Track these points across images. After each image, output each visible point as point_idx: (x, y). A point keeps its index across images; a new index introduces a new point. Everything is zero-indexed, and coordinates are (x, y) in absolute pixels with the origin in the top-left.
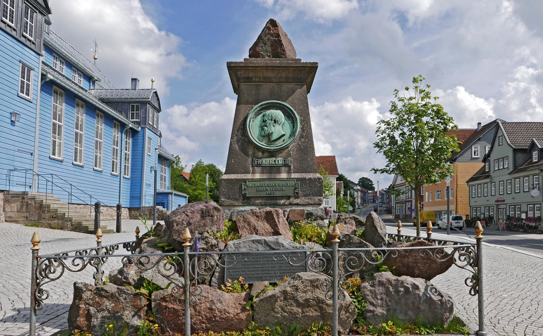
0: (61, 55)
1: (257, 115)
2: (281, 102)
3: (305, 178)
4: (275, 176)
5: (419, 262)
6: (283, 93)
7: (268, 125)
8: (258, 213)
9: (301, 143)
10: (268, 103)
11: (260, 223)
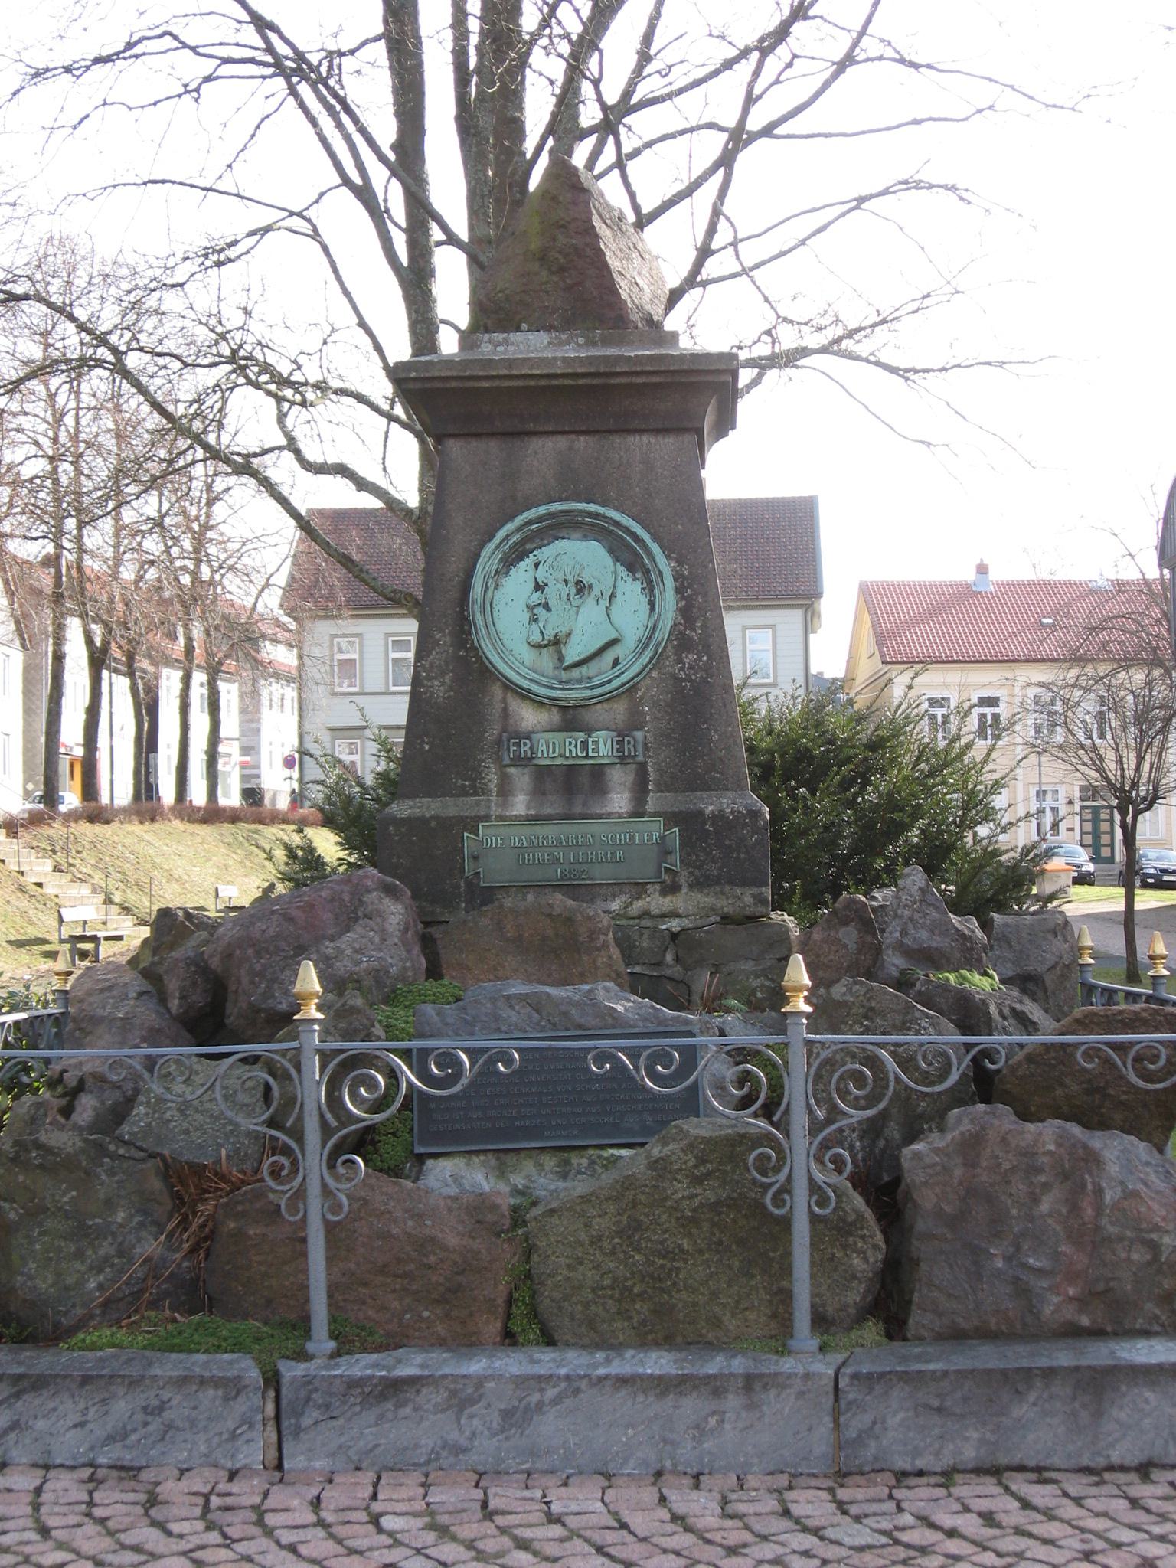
1: (513, 557)
2: (601, 510)
5: (1107, 1082)
10: (551, 515)
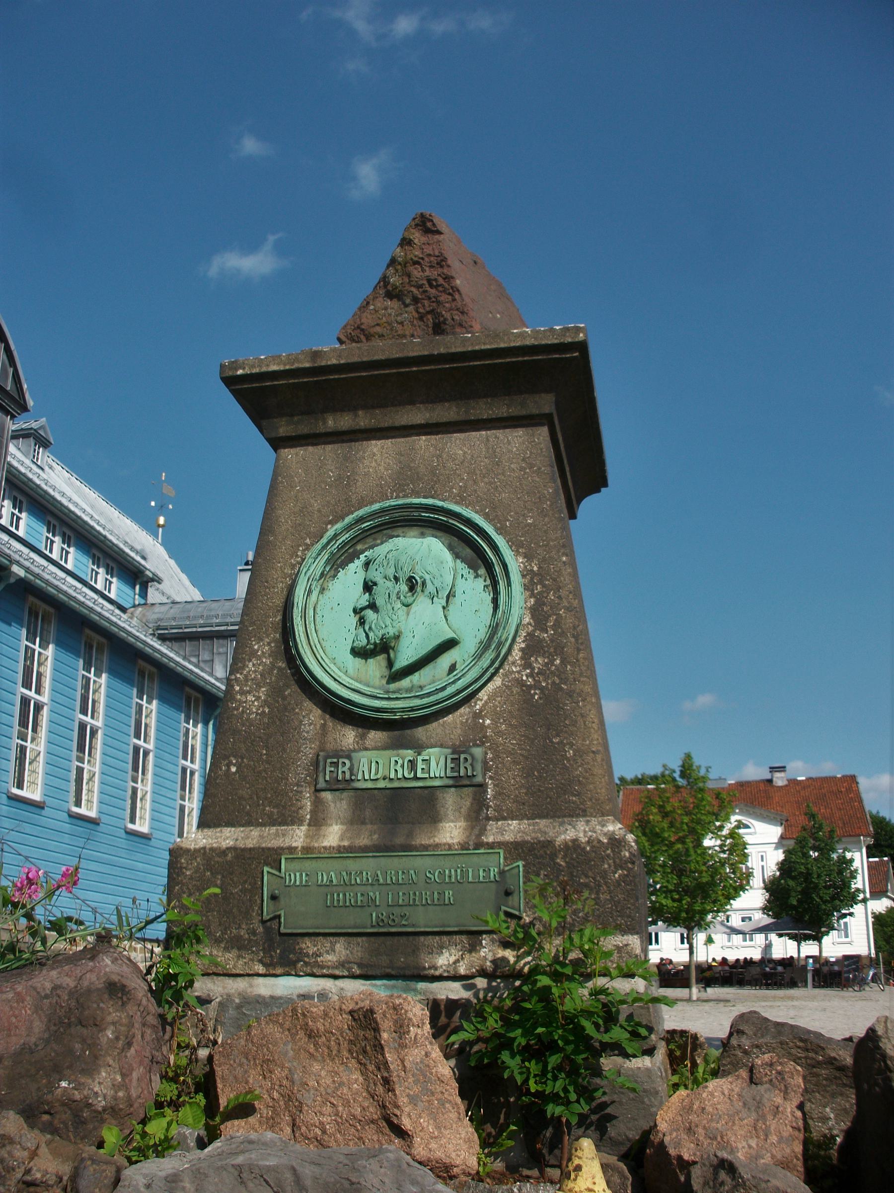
0: (64, 517)
3: (550, 843)
6: (450, 465)
7: (380, 602)
8: (314, 1020)
11: (316, 1067)
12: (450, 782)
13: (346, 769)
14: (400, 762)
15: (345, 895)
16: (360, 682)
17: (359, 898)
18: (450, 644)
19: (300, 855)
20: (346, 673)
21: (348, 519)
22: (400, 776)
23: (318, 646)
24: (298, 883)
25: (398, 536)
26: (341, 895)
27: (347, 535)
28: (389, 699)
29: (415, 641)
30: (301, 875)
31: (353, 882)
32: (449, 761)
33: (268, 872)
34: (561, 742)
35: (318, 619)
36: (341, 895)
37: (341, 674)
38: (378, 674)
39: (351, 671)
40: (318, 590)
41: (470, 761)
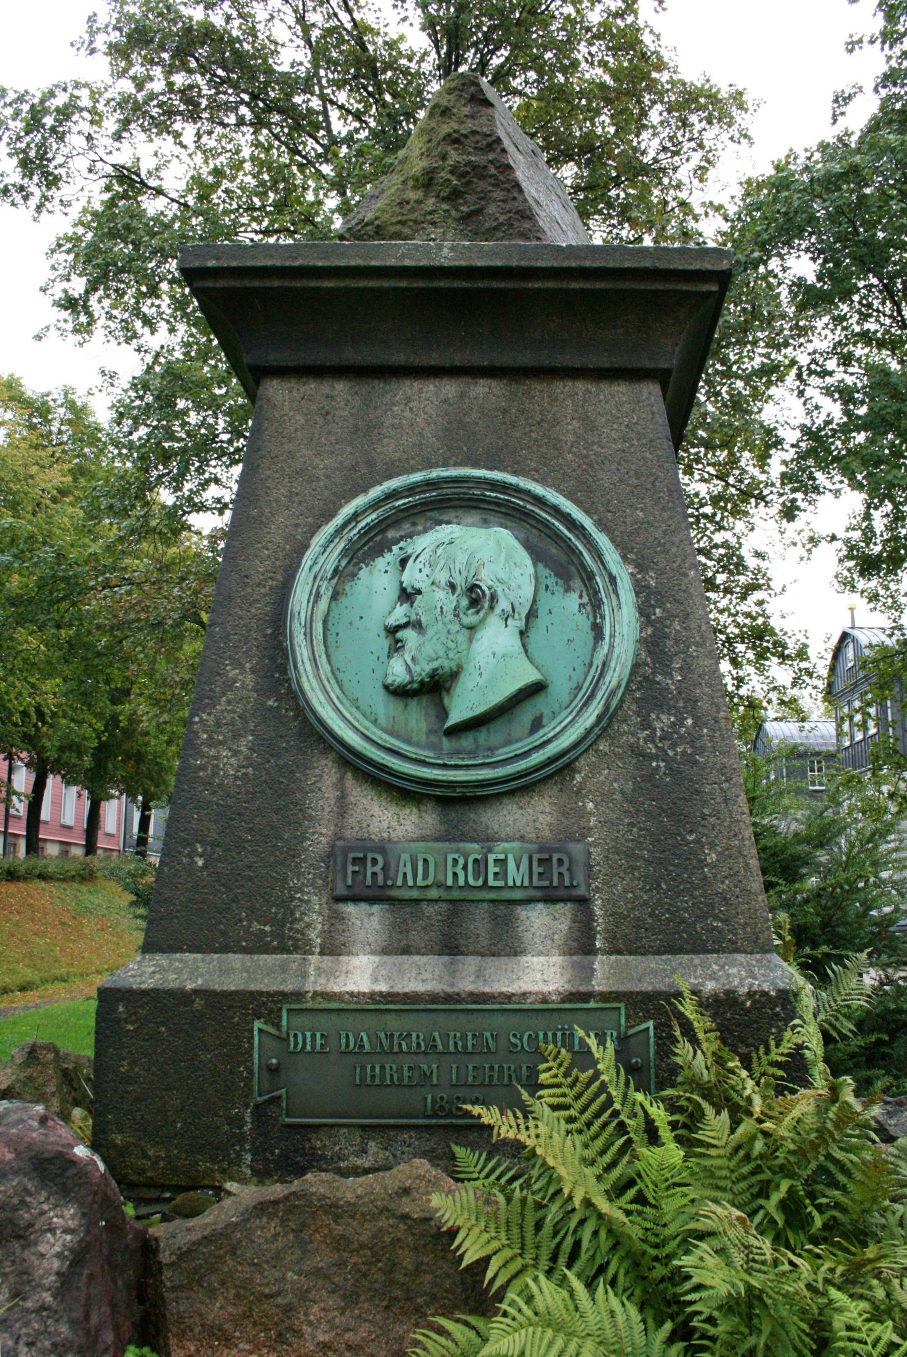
2: (537, 489)
4: (480, 973)
9: (651, 739)
12: (539, 894)
13: (378, 869)
14: (461, 861)
15: (383, 1068)
16: (398, 737)
17: (406, 1074)
18: (536, 689)
19: (310, 1005)
20: (375, 722)
21: (375, 492)
22: (461, 882)
23: (333, 681)
24: (309, 1048)
25: (448, 522)
26: (377, 1069)
27: (374, 516)
28: (445, 766)
29: (481, 681)
30: (313, 1036)
31: (396, 1049)
32: (535, 863)
33: (260, 1030)
34: (698, 841)
35: (331, 639)
36: (377, 1069)
37: (368, 724)
38: (424, 726)
39: (382, 720)
40: (329, 594)
41: (566, 864)
